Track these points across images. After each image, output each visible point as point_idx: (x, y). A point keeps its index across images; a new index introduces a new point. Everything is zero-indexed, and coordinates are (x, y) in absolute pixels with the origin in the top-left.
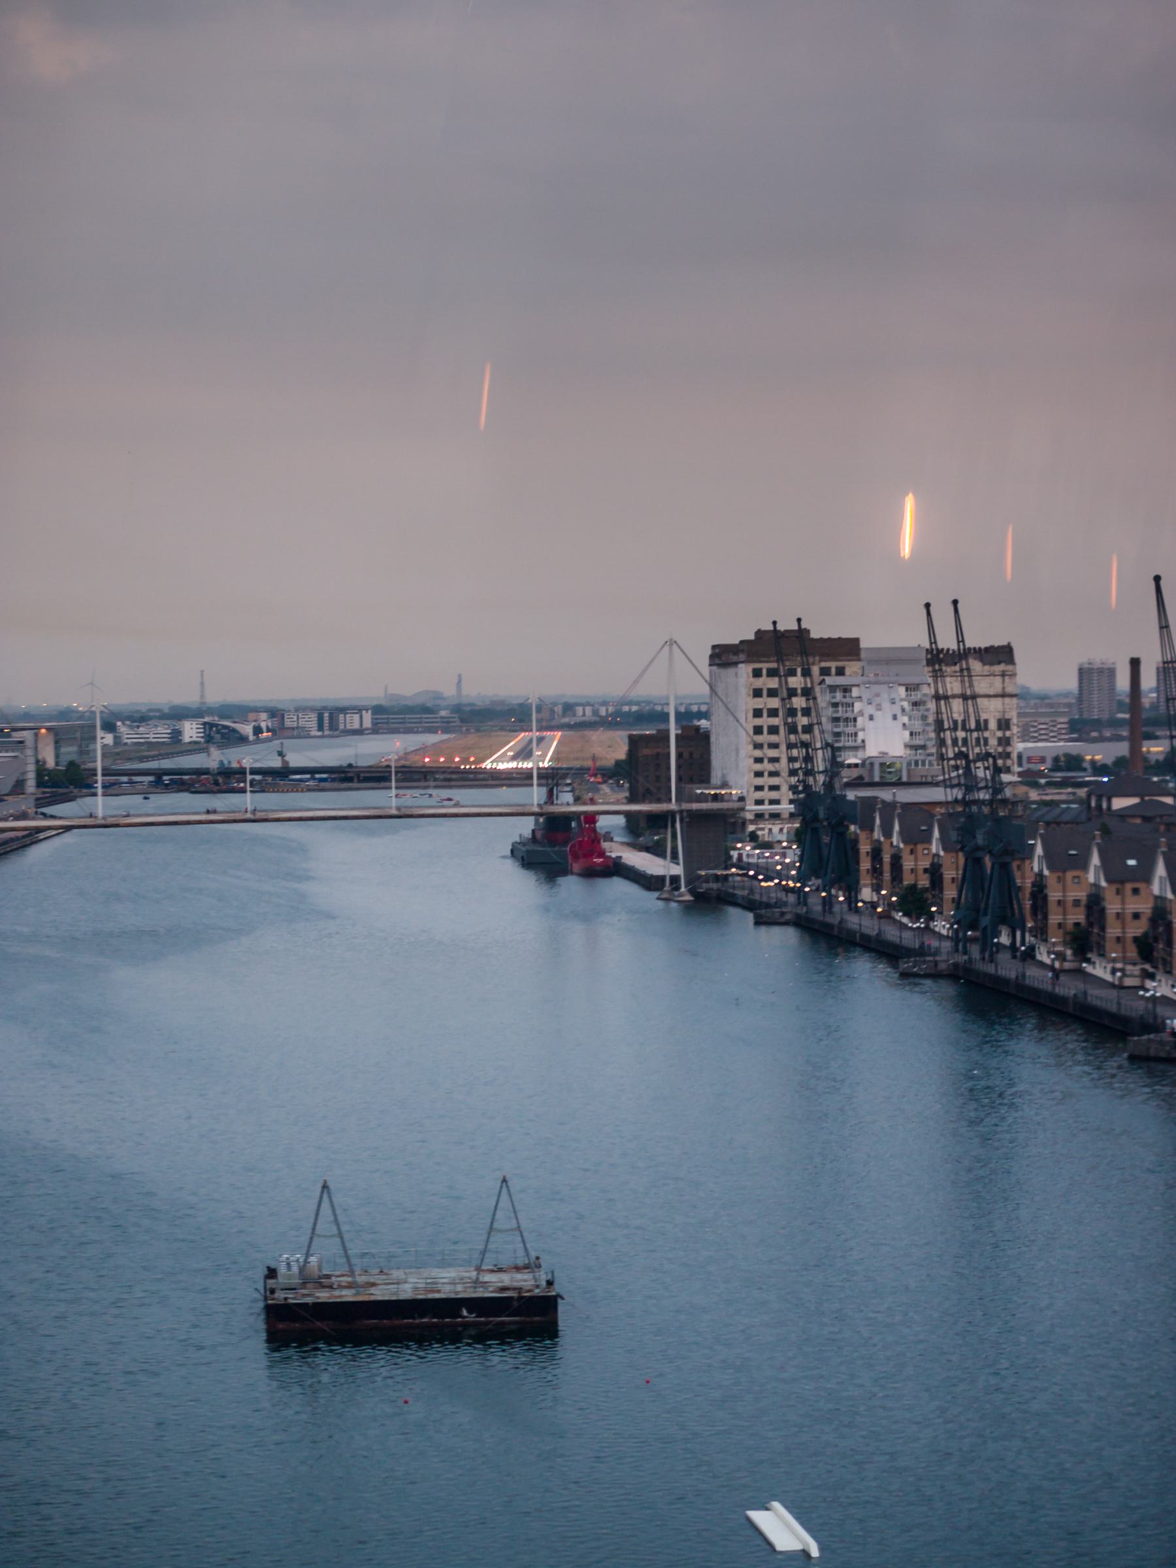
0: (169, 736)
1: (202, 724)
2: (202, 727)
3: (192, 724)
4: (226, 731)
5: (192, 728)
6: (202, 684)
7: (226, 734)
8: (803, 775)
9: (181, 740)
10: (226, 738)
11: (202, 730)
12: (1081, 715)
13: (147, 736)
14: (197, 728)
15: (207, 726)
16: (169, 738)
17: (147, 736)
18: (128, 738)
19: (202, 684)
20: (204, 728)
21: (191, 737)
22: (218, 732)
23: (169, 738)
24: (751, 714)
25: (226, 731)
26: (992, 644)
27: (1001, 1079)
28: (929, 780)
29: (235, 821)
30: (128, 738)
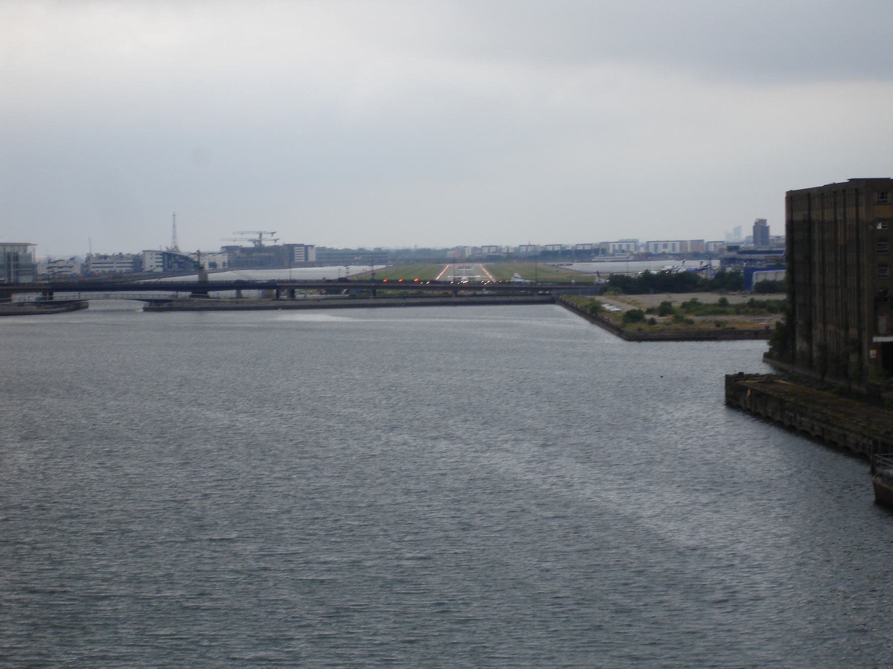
0: (131, 265)
1: (161, 255)
2: (161, 256)
3: (152, 254)
4: (183, 260)
5: (152, 258)
6: (174, 226)
7: (181, 263)
8: (597, 256)
9: (142, 269)
10: (181, 267)
11: (161, 260)
12: (648, 250)
13: (111, 265)
14: (156, 258)
15: (166, 257)
16: (131, 267)
17: (111, 265)
18: (93, 267)
19: (174, 226)
20: (163, 258)
21: (151, 266)
22: (176, 262)
23: (131, 267)
24: (212, 260)
25: (183, 260)
26: (361, 246)
27: (434, 450)
28: (661, 250)
29: (621, 261)
30: (93, 267)
